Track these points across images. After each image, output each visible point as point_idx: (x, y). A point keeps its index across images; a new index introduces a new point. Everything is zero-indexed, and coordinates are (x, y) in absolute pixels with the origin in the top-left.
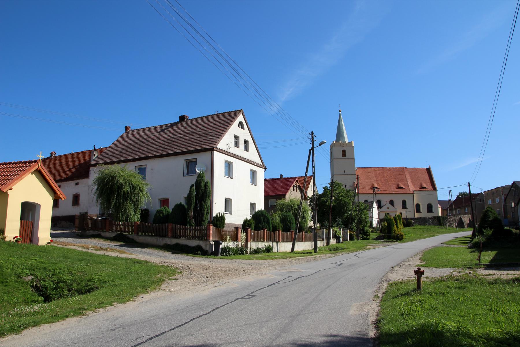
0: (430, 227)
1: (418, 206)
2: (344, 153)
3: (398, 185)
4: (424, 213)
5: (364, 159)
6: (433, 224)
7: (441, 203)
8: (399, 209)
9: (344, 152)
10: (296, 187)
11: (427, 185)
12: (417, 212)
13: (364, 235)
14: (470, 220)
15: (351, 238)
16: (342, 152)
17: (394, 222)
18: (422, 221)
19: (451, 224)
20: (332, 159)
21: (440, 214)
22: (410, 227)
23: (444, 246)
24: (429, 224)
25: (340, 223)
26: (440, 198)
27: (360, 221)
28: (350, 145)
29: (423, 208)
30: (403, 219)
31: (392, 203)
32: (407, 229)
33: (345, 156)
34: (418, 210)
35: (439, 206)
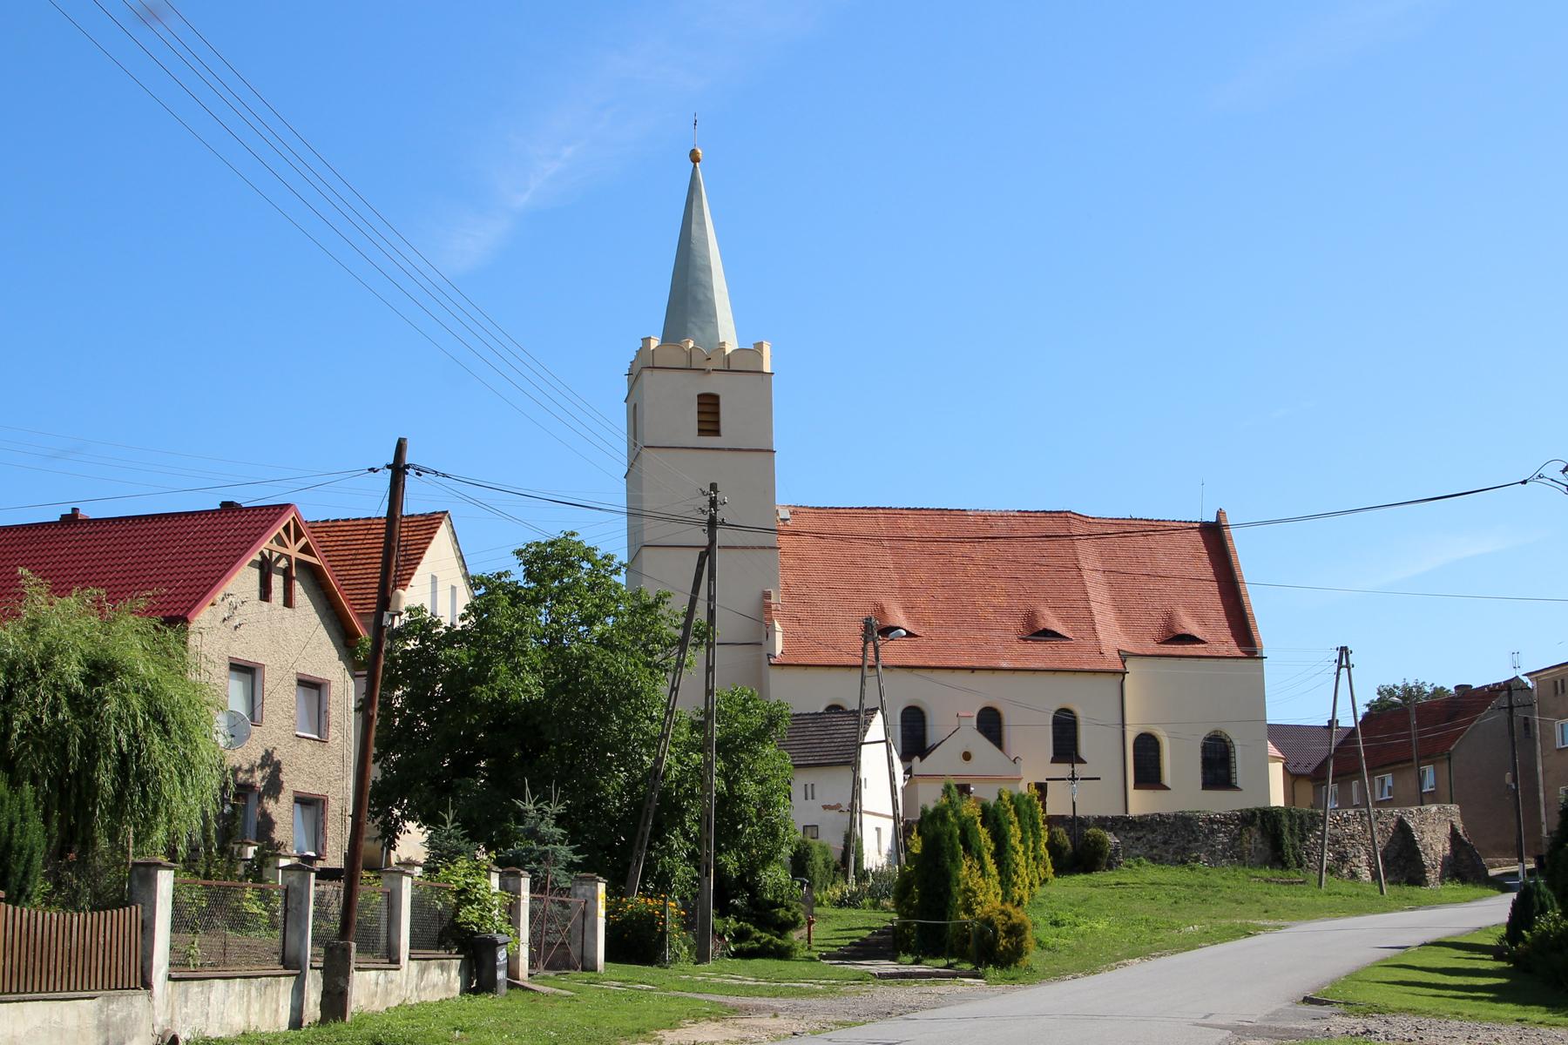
0: (1216, 877)
1: (1147, 748)
2: (709, 411)
3: (1031, 618)
4: (1182, 790)
5: (826, 456)
6: (1236, 856)
7: (1283, 735)
8: (1030, 757)
9: (709, 407)
10: (286, 573)
11: (1203, 622)
12: (1139, 784)
13: (754, 922)
14: (1454, 834)
15: (635, 943)
16: (698, 402)
17: (984, 834)
18: (1172, 840)
19: (1342, 858)
20: (638, 446)
21: (1277, 799)
22: (1096, 877)
23: (1340, 1023)
24: (1214, 858)
25: (548, 828)
26: (1277, 714)
27: (728, 818)
28: (746, 366)
29: (1180, 764)
30: (1052, 821)
31: (991, 724)
32: (1076, 885)
33: (717, 432)
34: (1148, 772)
35: (1272, 750)
